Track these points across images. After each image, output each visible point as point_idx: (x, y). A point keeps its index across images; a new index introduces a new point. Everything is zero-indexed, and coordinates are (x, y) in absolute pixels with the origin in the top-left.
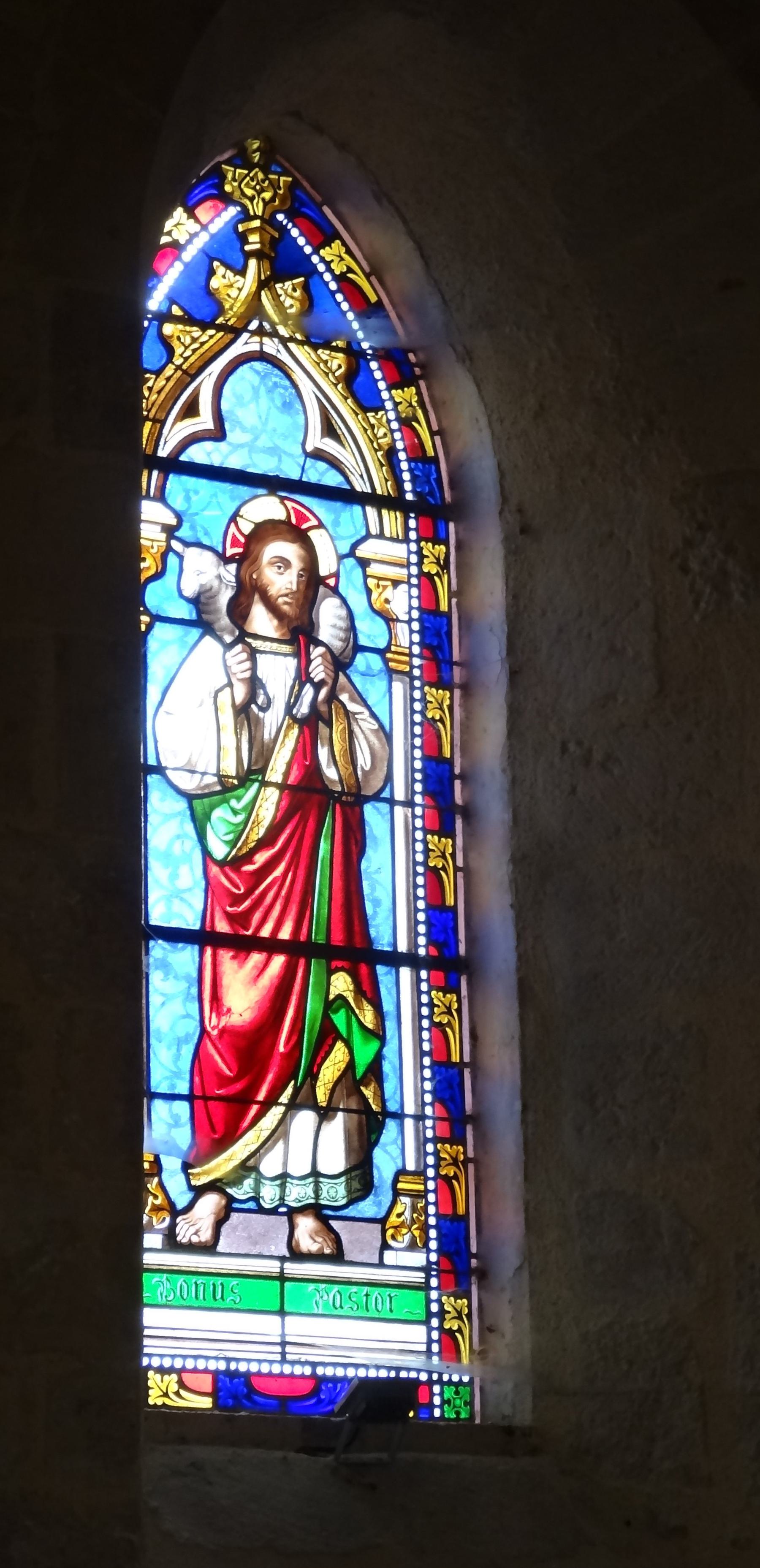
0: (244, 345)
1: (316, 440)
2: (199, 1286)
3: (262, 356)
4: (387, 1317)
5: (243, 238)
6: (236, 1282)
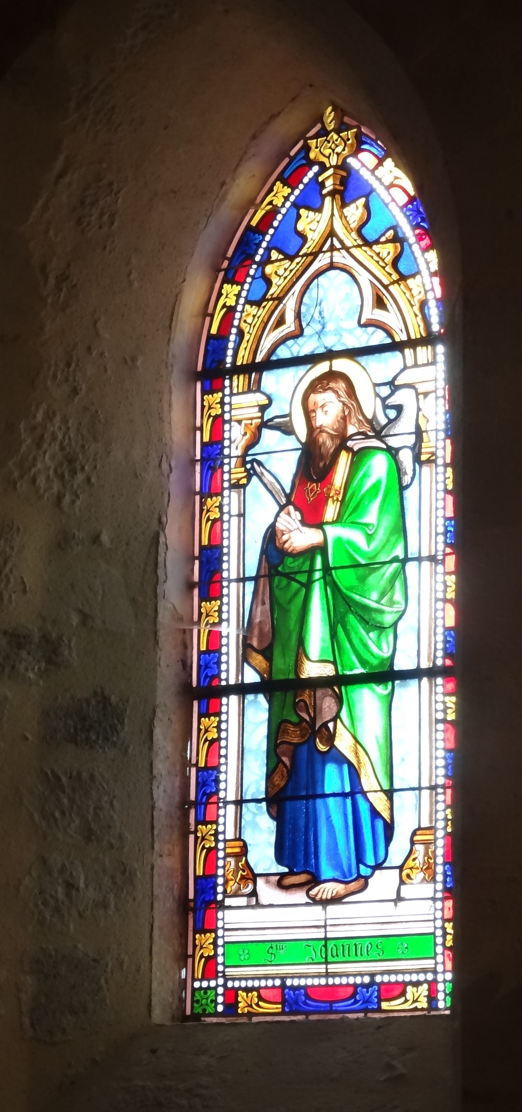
0: (323, 260)
1: (370, 313)
2: (358, 946)
3: (332, 266)
4: (366, 959)
5: (322, 185)
6: (380, 941)
